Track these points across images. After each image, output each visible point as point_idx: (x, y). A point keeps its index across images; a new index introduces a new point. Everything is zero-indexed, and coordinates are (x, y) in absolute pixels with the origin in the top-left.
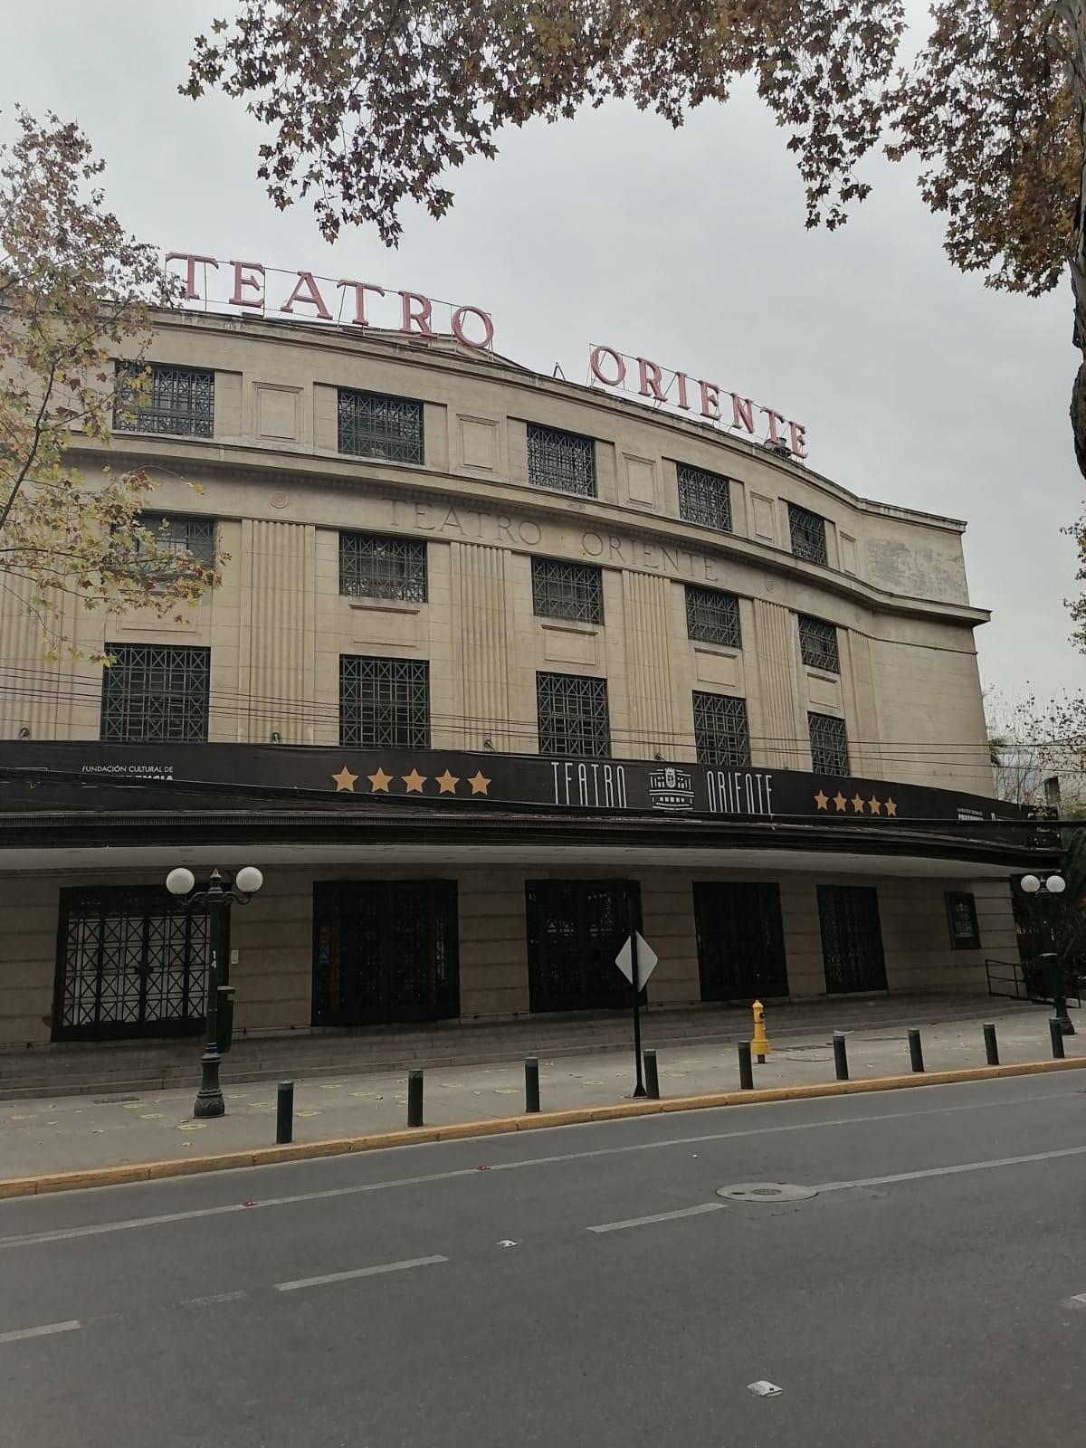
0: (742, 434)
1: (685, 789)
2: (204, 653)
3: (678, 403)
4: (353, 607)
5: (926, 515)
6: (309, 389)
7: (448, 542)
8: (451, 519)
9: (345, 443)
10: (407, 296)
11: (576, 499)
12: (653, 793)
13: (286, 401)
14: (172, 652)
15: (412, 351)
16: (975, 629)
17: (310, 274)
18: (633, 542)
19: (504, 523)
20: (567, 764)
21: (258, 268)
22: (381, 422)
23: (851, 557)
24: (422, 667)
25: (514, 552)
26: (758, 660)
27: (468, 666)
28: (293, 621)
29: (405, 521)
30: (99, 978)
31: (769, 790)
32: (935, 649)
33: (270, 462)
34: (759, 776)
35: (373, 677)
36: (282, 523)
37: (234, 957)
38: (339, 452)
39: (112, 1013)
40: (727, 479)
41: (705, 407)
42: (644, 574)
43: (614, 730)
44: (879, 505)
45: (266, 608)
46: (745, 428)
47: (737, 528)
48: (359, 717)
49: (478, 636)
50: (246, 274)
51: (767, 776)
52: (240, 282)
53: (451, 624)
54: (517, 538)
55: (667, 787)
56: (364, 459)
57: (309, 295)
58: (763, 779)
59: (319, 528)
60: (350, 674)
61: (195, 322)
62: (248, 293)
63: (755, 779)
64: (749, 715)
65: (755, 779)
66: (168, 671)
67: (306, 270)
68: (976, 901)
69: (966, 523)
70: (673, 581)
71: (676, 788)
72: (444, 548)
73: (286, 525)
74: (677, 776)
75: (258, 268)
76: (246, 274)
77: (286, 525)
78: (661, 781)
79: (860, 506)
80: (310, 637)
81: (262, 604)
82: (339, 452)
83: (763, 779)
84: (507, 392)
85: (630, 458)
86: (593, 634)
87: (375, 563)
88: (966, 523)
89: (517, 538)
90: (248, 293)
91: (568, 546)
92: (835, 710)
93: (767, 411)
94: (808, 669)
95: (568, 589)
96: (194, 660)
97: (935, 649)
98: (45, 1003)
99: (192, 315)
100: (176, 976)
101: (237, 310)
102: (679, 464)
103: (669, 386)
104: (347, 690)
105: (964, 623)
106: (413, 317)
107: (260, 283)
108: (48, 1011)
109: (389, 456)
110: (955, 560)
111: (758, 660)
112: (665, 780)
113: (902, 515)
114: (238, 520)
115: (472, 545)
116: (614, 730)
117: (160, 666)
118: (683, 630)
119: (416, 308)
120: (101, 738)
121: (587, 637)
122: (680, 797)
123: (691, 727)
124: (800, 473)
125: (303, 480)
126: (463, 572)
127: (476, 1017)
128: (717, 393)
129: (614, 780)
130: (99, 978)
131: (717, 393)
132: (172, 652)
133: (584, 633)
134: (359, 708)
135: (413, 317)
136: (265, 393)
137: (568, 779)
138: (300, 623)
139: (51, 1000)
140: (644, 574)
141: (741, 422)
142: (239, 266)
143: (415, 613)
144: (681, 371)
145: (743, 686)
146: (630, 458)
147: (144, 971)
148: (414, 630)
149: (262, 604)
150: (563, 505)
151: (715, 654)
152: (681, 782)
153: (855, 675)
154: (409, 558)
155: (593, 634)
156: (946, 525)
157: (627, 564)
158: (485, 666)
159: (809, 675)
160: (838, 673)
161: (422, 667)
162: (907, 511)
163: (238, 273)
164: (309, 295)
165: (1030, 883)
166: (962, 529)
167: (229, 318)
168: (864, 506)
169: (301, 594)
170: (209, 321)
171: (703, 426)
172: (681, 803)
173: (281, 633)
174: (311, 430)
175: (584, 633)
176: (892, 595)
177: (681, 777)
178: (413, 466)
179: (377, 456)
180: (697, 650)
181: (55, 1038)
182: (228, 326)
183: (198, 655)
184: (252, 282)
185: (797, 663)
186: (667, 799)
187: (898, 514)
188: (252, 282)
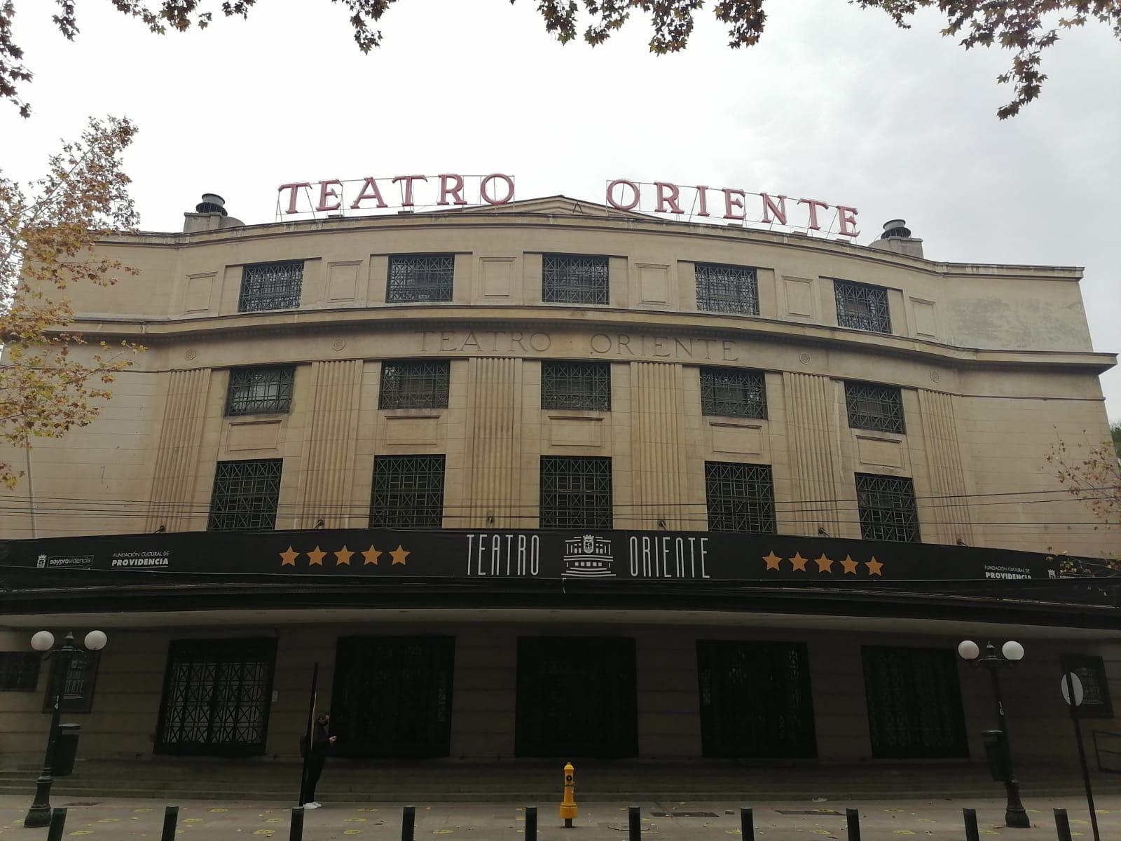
0: (777, 227)
1: (603, 554)
2: (607, 462)
3: (724, 213)
4: (389, 418)
5: (1027, 268)
6: (674, 264)
7: (466, 359)
8: (471, 341)
9: (547, 294)
10: (660, 186)
11: (578, 309)
12: (567, 558)
13: (351, 270)
14: (721, 467)
15: (445, 217)
16: (1100, 376)
17: (372, 178)
18: (643, 337)
19: (517, 337)
20: (481, 536)
21: (742, 193)
22: (577, 275)
23: (910, 322)
24: (440, 460)
25: (525, 359)
26: (787, 429)
27: (478, 456)
28: (341, 433)
29: (432, 346)
30: (237, 708)
31: (665, 551)
32: (1045, 399)
33: (328, 318)
34: (692, 539)
35: (414, 471)
36: (340, 361)
37: (275, 696)
38: (543, 301)
39: (245, 736)
40: (755, 269)
41: (729, 210)
42: (654, 363)
43: (536, 506)
44: (964, 266)
45: (323, 425)
46: (777, 220)
47: (765, 311)
48: (583, 505)
49: (488, 431)
50: (734, 197)
51: (664, 538)
52: (729, 203)
53: (466, 423)
54: (528, 347)
55: (583, 553)
56: (600, 306)
57: (366, 193)
58: (697, 544)
59: (366, 361)
60: (549, 470)
61: (292, 229)
62: (736, 211)
63: (687, 544)
64: (775, 481)
65: (687, 544)
66: (758, 482)
67: (369, 176)
68: (1105, 665)
69: (1082, 269)
70: (685, 365)
71: (594, 553)
72: (624, 368)
73: (657, 364)
74: (595, 542)
75: (742, 193)
76: (734, 197)
77: (657, 364)
78: (578, 547)
79: (939, 270)
80: (352, 444)
81: (320, 423)
82: (543, 301)
83: (697, 544)
84: (525, 233)
85: (642, 266)
86: (600, 420)
87: (582, 383)
88: (1082, 269)
89: (528, 347)
90: (736, 211)
91: (577, 348)
92: (898, 470)
93: (804, 201)
94: (857, 432)
95: (416, 384)
96: (587, 467)
97: (1045, 399)
98: (151, 724)
99: (290, 225)
100: (205, 708)
101: (323, 215)
102: (696, 263)
103: (688, 201)
104: (546, 483)
105: (1090, 370)
106: (665, 200)
107: (742, 203)
108: (153, 730)
109: (431, 299)
110: (1070, 307)
111: (787, 429)
112: (582, 547)
113: (996, 272)
114: (309, 363)
115: (487, 358)
116: (536, 506)
117: (591, 472)
118: (698, 408)
119: (667, 193)
120: (540, 526)
121: (593, 423)
122: (598, 562)
123: (702, 494)
124: (848, 250)
125: (651, 330)
126: (478, 380)
127: (462, 758)
128: (744, 196)
129: (528, 549)
130: (237, 708)
131: (744, 196)
132: (721, 467)
133: (590, 419)
134: (387, 496)
135: (665, 200)
136: (337, 269)
137: (481, 549)
138: (346, 434)
139: (155, 724)
140: (654, 363)
141: (771, 215)
142: (727, 192)
143: (437, 417)
144: (700, 184)
145: (907, 467)
146: (642, 266)
147: (213, 705)
148: (442, 433)
149: (320, 423)
150: (566, 315)
151: (735, 426)
152: (600, 547)
153: (927, 432)
154: (596, 378)
155: (600, 420)
156: (1056, 274)
157: (638, 356)
158: (492, 455)
159: (858, 437)
160: (904, 433)
161: (440, 460)
162: (1001, 267)
163: (728, 198)
164: (366, 193)
165: (968, 649)
166: (1077, 275)
167: (313, 222)
168: (945, 270)
169: (348, 412)
170: (301, 226)
171: (731, 227)
172: (598, 567)
173: (332, 444)
174: (818, 309)
175: (590, 419)
176: (977, 351)
177: (599, 543)
178: (443, 303)
179: (423, 300)
180: (713, 424)
181: (156, 751)
182: (313, 227)
183: (396, 462)
184: (738, 203)
185: (841, 427)
186: (582, 564)
187: (990, 272)
188: (333, 193)
